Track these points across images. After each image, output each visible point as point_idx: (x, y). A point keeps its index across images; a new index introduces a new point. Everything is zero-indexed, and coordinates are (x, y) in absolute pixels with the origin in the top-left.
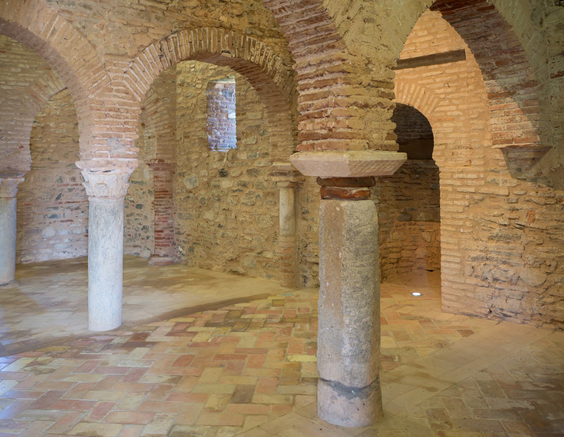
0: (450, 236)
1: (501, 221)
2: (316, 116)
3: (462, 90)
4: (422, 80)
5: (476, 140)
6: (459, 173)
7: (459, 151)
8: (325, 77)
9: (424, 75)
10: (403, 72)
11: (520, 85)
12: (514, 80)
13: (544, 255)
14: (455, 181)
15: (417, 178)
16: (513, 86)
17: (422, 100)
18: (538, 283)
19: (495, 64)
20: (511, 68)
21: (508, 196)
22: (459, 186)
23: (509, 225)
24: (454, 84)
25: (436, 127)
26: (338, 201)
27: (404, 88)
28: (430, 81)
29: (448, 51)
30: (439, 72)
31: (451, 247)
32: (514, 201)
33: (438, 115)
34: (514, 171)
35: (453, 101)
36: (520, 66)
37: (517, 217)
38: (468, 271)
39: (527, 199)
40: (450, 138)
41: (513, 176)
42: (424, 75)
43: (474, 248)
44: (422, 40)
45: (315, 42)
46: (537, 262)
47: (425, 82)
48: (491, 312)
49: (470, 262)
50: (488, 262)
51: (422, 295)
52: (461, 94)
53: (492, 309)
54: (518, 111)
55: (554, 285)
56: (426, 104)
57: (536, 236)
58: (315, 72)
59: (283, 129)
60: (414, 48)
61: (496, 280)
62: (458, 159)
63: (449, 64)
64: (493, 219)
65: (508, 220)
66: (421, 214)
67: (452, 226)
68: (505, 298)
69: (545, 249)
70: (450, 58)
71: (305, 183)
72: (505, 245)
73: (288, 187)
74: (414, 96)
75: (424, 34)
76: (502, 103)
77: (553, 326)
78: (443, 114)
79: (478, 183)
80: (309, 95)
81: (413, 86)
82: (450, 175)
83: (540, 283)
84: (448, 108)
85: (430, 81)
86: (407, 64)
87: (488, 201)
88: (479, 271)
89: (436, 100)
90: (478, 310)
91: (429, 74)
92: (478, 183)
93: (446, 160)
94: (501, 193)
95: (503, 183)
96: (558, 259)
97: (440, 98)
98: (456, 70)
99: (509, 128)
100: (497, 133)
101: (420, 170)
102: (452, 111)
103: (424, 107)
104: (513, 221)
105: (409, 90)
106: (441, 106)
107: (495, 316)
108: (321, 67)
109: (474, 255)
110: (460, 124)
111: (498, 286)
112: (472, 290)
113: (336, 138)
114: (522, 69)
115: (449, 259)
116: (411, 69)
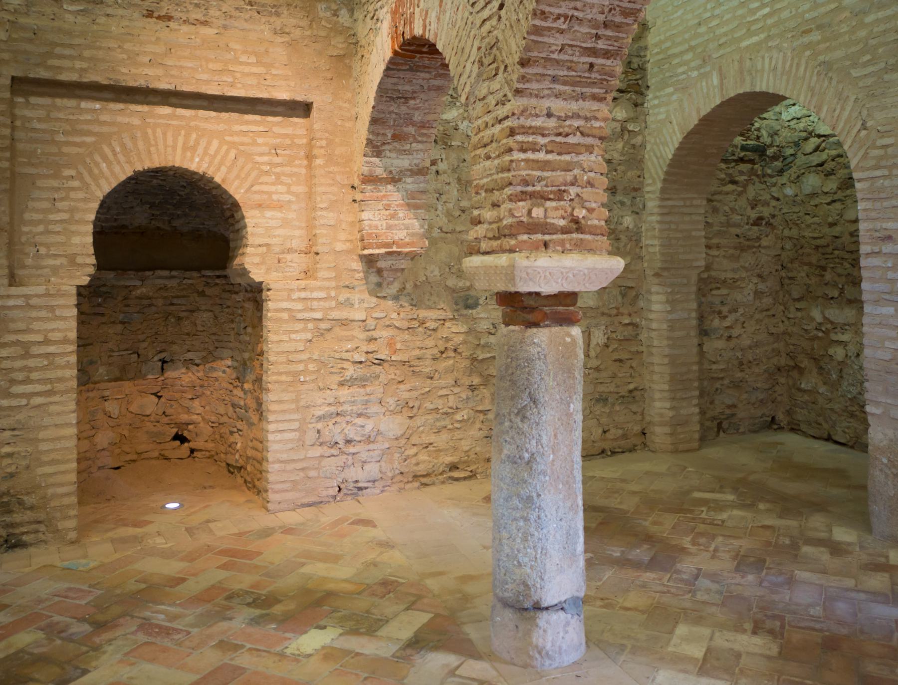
0: (283, 391)
1: (358, 357)
2: (552, 196)
3: (297, 162)
4: (231, 135)
5: (325, 241)
6: (300, 290)
7: (289, 257)
8: (571, 140)
9: (237, 128)
11: (411, 170)
12: (404, 162)
13: (406, 395)
14: (293, 304)
15: (99, 305)
16: (401, 171)
17: (230, 170)
18: (399, 433)
19: (389, 137)
20: (407, 147)
21: (364, 321)
22: (300, 311)
24: (285, 152)
25: (253, 217)
26: (565, 329)
27: (197, 143)
28: (246, 140)
29: (288, 99)
32: (373, 327)
33: (257, 197)
34: (373, 286)
35: (283, 178)
36: (420, 146)
38: (311, 436)
39: (388, 323)
40: (275, 236)
41: (372, 293)
42: (237, 128)
44: (247, 69)
45: (574, 84)
47: (236, 139)
48: (340, 489)
49: (313, 425)
50: (338, 419)
51: (181, 506)
52: (295, 170)
53: (342, 486)
54: (402, 205)
56: (238, 177)
57: (398, 372)
58: (556, 128)
60: (231, 80)
61: (348, 442)
62: (287, 269)
63: (279, 119)
64: (345, 355)
65: (364, 355)
66: (101, 371)
67: (287, 373)
68: (360, 464)
69: (407, 386)
70: (279, 109)
72: (362, 390)
74: (217, 161)
75: (250, 61)
76: (379, 191)
77: (416, 484)
78: (265, 197)
79: (326, 304)
80: (537, 161)
81: (215, 143)
82: (286, 294)
83: (401, 432)
84: (273, 188)
85: (246, 140)
86: (205, 103)
87: (339, 331)
88: (327, 436)
89: (254, 174)
90: (325, 493)
91: (244, 128)
92: (326, 304)
93: (268, 270)
95: (359, 303)
96: (420, 397)
97: (262, 171)
98: (289, 131)
99: (389, 227)
100: (371, 233)
101: (103, 289)
102: (281, 193)
104: (371, 355)
105: (206, 149)
106: (262, 183)
107: (346, 494)
108: (568, 123)
109: (319, 412)
110: (291, 215)
111: (352, 450)
112: (316, 466)
113: (591, 233)
114: (421, 150)
115: (281, 426)
116: (213, 114)
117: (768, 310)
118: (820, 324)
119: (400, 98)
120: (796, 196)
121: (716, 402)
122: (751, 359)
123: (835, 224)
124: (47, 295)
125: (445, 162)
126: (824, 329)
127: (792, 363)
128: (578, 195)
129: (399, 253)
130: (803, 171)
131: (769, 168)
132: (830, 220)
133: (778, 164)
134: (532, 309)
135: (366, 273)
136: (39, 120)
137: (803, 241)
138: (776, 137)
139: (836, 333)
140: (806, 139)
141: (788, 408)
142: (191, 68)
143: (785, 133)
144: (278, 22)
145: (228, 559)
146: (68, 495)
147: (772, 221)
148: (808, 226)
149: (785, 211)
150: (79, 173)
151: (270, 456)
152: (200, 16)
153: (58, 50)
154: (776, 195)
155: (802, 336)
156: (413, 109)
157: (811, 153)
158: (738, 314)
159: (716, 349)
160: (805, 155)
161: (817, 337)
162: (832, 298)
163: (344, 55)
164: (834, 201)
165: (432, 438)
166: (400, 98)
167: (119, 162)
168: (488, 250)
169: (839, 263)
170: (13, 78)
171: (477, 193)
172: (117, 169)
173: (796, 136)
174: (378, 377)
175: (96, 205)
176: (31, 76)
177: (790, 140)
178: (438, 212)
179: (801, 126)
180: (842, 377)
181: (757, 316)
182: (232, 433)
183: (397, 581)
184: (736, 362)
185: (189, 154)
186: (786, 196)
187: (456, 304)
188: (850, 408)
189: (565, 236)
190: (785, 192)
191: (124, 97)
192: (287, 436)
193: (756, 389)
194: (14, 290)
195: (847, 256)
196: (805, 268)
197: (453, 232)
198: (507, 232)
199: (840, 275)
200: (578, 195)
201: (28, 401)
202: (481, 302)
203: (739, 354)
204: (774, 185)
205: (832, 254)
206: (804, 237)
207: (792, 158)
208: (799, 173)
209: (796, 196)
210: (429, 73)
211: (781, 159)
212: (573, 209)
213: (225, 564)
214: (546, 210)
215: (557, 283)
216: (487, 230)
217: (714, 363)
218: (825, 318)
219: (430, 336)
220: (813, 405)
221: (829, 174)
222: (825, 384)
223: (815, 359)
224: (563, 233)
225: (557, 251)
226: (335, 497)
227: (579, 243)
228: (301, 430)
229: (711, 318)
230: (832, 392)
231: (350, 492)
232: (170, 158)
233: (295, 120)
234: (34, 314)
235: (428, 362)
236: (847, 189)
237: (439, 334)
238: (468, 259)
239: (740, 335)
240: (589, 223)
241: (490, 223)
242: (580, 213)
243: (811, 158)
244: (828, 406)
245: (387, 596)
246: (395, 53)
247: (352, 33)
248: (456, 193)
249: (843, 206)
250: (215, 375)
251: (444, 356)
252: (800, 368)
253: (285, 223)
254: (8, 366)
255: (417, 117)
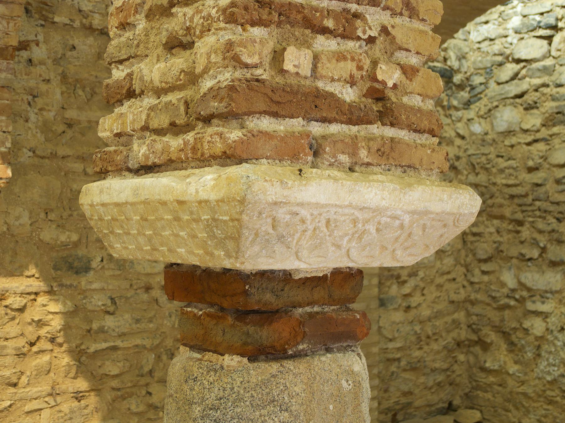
2: (330, 23)
117: (449, 273)
118: (513, 290)
120: (486, 134)
121: (392, 389)
122: (430, 333)
123: (537, 169)
125: (43, 47)
126: (517, 296)
127: (474, 337)
128: (384, 30)
130: (495, 104)
131: (455, 98)
132: (531, 163)
133: (464, 95)
134: (268, 315)
137: (494, 189)
138: (464, 61)
139: (534, 302)
140: (500, 65)
141: (467, 390)
143: (473, 57)
147: (457, 164)
148: (502, 171)
149: (469, 152)
154: (461, 132)
155: (488, 304)
157: (507, 82)
158: (418, 278)
159: (394, 322)
160: (499, 84)
161: (508, 307)
162: (530, 259)
164: (536, 141)
168: (153, 159)
169: (540, 217)
171: (124, 26)
173: (488, 61)
177: (481, 66)
178: (30, 125)
179: (497, 47)
180: (539, 355)
181: (439, 280)
184: (413, 339)
186: (472, 134)
187: (56, 268)
188: (549, 393)
189: (354, 129)
190: (472, 128)
193: (433, 370)
195: (552, 208)
196: (495, 222)
197: (53, 155)
198: (215, 106)
199: (541, 232)
200: (384, 30)
202: (94, 264)
203: (417, 328)
204: (460, 120)
205: (530, 205)
206: (494, 184)
207: (483, 87)
208: (490, 106)
209: (486, 134)
211: (468, 89)
212: (375, 63)
214: (316, 58)
215: (339, 247)
216: (152, 108)
217: (391, 340)
218: (521, 284)
219: (13, 319)
220: (500, 389)
221: (529, 108)
222: (516, 363)
223: (504, 333)
224: (350, 122)
225: (338, 165)
227: (387, 149)
229: (388, 283)
230: (526, 374)
236: (554, 125)
237: (27, 316)
238: (95, 186)
239: (419, 305)
240: (405, 99)
241: (159, 92)
242: (389, 75)
243: (507, 87)
244: (520, 390)
248: (58, 96)
249: (548, 147)
251: (35, 349)
252: (485, 342)
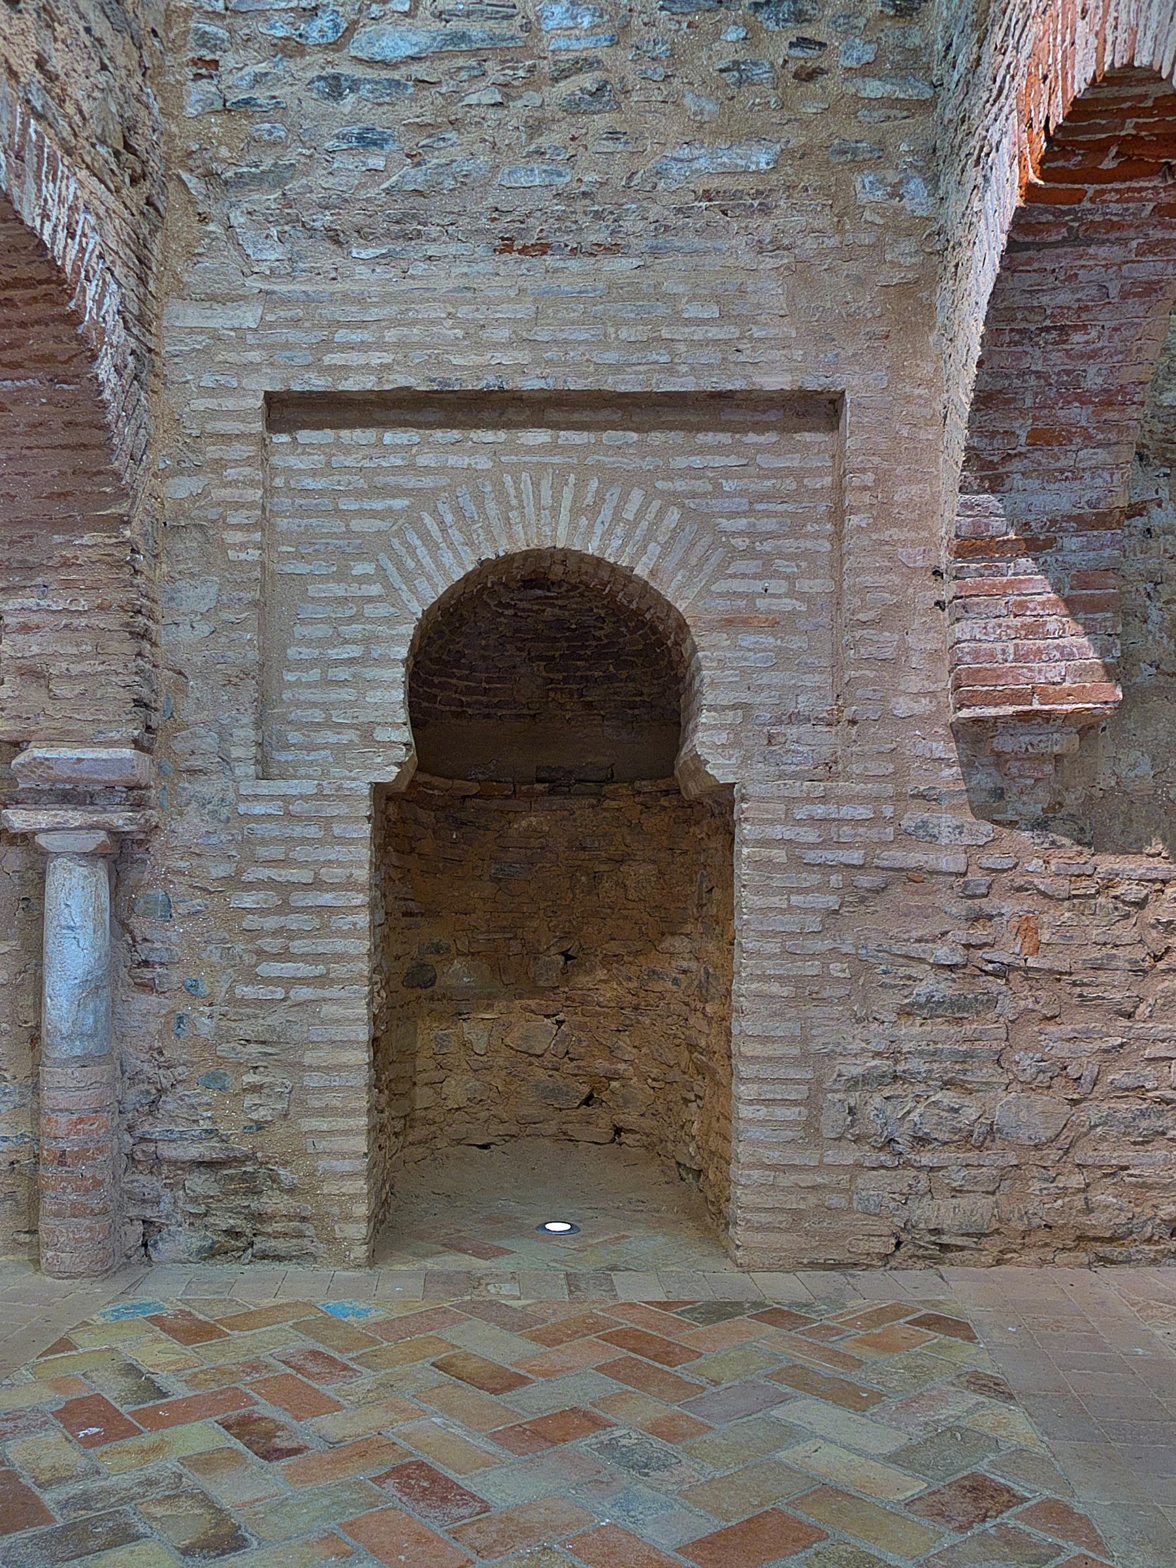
0: (773, 1015)
1: (943, 953)
7: (793, 731)
9: (680, 462)
10: (599, 442)
11: (1078, 519)
14: (798, 829)
16: (1053, 522)
18: (1045, 1134)
19: (1023, 440)
21: (965, 874)
23: (965, 966)
27: (600, 497)
30: (733, 461)
31: (779, 1050)
32: (984, 890)
36: (1102, 455)
37: (990, 940)
38: (832, 1120)
39: (1020, 881)
41: (981, 812)
42: (680, 462)
43: (857, 1045)
44: (699, 334)
46: (1044, 1072)
47: (680, 485)
50: (898, 1089)
53: (904, 1236)
55: (1086, 1134)
59: (83, 604)
60: (665, 359)
61: (921, 1141)
63: (771, 437)
64: (916, 949)
70: (771, 416)
71: (157, 842)
73: (90, 857)
77: (1084, 1258)
79: (873, 834)
81: (637, 496)
83: (1051, 1133)
90: (864, 1246)
91: (697, 461)
92: (873, 834)
94: (943, 866)
103: (674, 573)
106: (733, 576)
109: (856, 1070)
111: (926, 1159)
119: (1047, 329)
124: (319, 796)
129: (1048, 716)
135: (968, 766)
136: (314, 473)
142: (585, 342)
144: (766, 227)
145: (623, 1353)
146: (352, 1175)
150: (380, 568)
151: (742, 1151)
152: (603, 237)
153: (341, 335)
156: (1081, 356)
163: (917, 281)
165: (1128, 1155)
166: (1047, 329)
167: (451, 545)
170: (269, 397)
172: (448, 558)
174: (992, 1002)
175: (408, 630)
176: (296, 387)
182: (686, 1101)
183: (1009, 1490)
185: (584, 521)
191: (460, 417)
192: (781, 1113)
194: (264, 788)
201: (287, 993)
210: (1123, 242)
213: (614, 1364)
219: (1127, 916)
226: (885, 1258)
228: (811, 1102)
231: (921, 1252)
232: (547, 530)
233: (808, 437)
234: (298, 831)
235: (1119, 977)
245: (977, 1528)
246: (1030, 191)
247: (936, 227)
250: (658, 987)
251: (1161, 965)
253: (783, 659)
254: (256, 926)
255: (1093, 380)
